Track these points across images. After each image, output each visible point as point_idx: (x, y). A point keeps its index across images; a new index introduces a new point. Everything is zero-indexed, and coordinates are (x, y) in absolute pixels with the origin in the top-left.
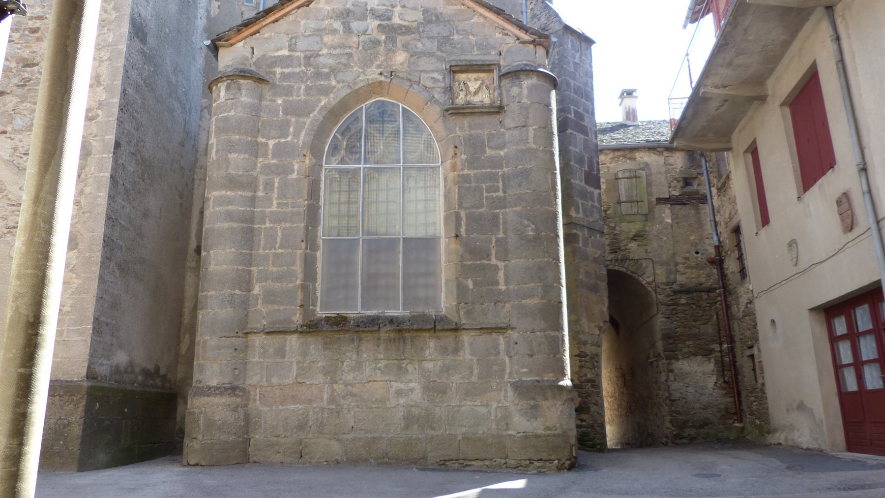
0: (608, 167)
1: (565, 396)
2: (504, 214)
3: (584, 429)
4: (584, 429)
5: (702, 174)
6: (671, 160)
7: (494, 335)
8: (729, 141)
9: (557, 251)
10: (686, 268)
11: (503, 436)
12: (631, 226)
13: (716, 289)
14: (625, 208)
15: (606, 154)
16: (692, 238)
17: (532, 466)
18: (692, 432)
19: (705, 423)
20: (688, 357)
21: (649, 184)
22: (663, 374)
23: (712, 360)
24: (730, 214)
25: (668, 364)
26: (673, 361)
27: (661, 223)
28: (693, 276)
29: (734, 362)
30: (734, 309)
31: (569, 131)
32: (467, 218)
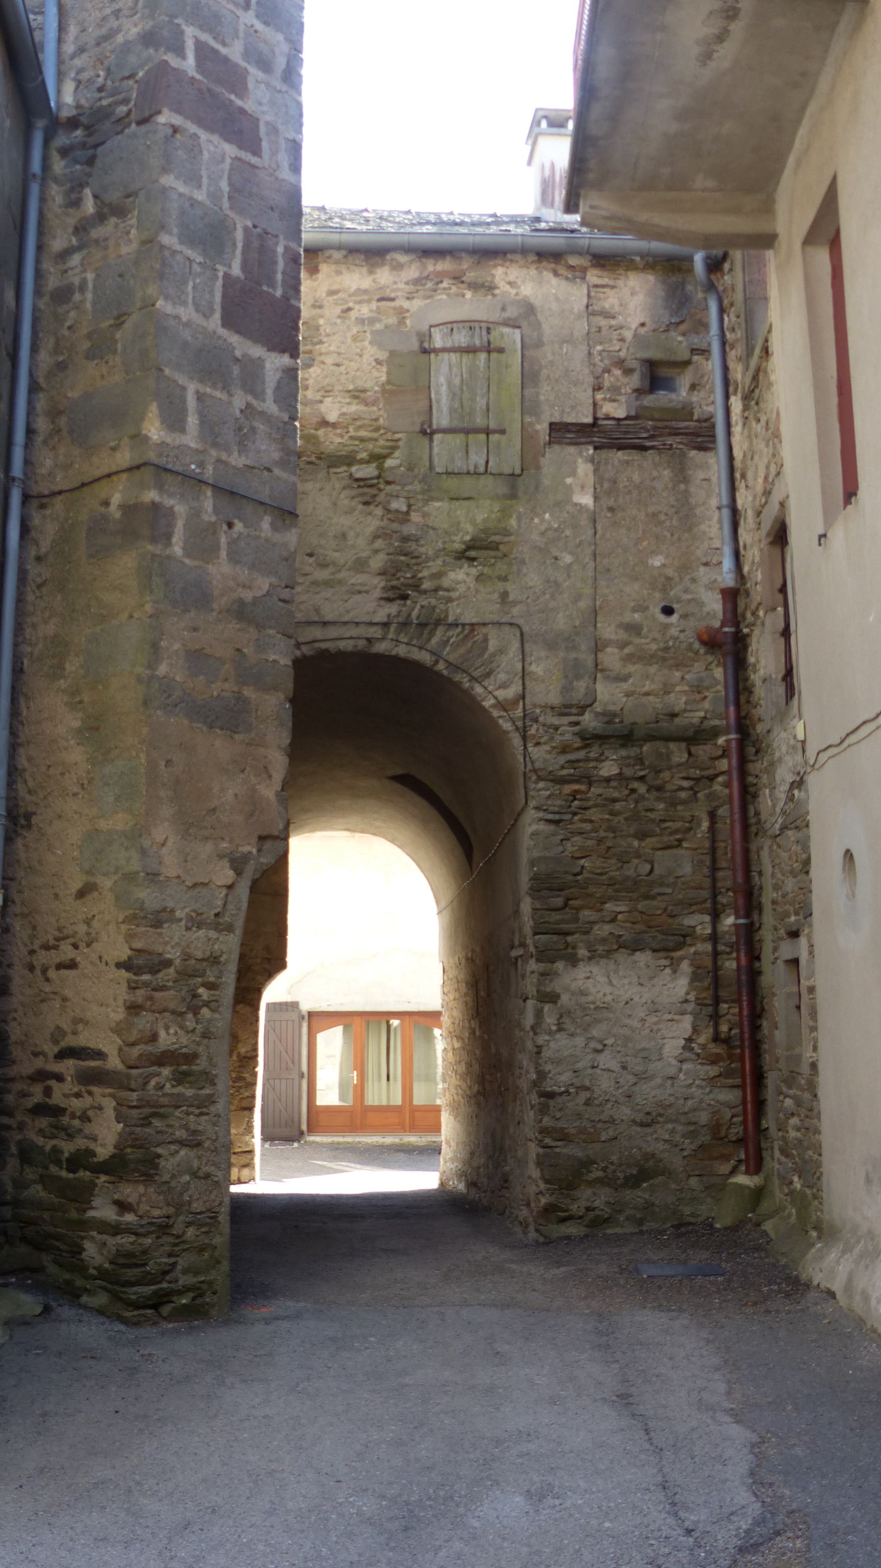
0: (401, 313)
3: (125, 1241)
4: (125, 1241)
5: (705, 352)
6: (610, 300)
8: (767, 208)
10: (629, 658)
12: (461, 510)
13: (715, 733)
14: (444, 451)
15: (398, 267)
16: (657, 561)
18: (599, 1199)
19: (644, 1172)
20: (608, 954)
21: (530, 376)
22: (530, 1003)
23: (685, 966)
24: (766, 478)
25: (542, 974)
26: (560, 965)
28: (648, 686)
29: (752, 973)
31: (165, 118)
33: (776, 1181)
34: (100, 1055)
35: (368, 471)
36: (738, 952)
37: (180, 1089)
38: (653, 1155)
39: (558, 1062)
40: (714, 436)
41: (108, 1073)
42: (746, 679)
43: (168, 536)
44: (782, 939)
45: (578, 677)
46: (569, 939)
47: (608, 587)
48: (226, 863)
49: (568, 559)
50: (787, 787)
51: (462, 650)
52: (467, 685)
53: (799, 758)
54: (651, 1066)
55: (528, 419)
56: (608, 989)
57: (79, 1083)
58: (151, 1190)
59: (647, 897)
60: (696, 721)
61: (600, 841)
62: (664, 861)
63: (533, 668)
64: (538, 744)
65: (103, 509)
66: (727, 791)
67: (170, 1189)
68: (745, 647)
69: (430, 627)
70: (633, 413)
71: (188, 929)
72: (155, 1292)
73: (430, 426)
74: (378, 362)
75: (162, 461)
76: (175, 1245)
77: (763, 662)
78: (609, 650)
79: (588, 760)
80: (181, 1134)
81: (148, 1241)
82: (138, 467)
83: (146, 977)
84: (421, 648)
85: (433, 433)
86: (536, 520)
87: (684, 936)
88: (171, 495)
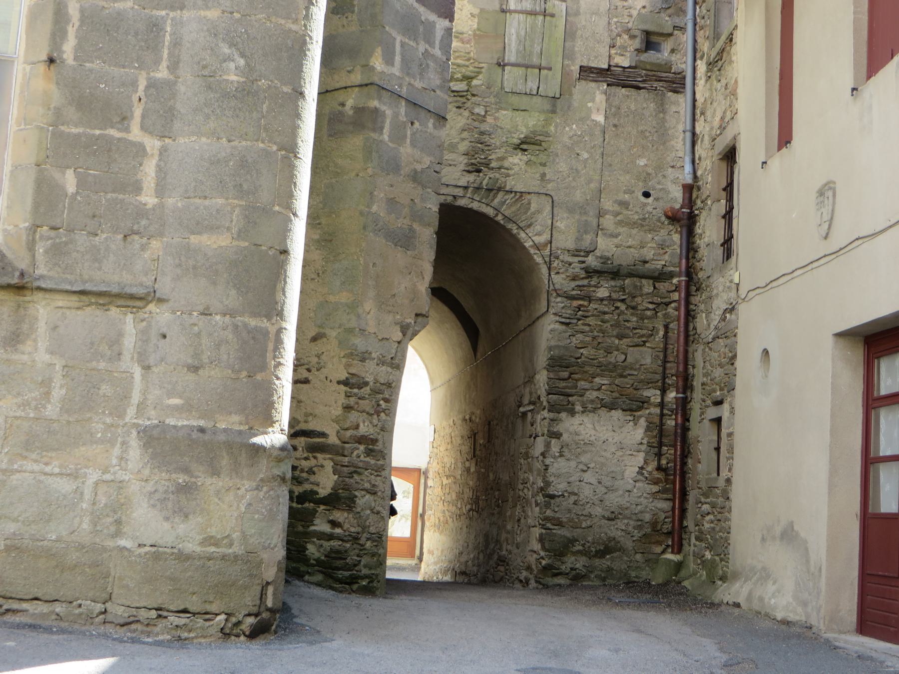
1: (264, 469)
2: (176, 23)
3: (335, 543)
4: (335, 543)
5: (682, 29)
7: (114, 312)
9: (294, 131)
10: (620, 223)
11: (105, 549)
12: (519, 117)
13: (671, 275)
14: (511, 78)
16: (642, 162)
17: (161, 624)
18: (580, 563)
19: (608, 549)
20: (594, 410)
21: (570, 34)
22: (540, 440)
24: (722, 119)
26: (563, 415)
27: (583, 120)
29: (684, 429)
30: (701, 321)
32: (82, 21)
33: (691, 558)
34: (323, 435)
35: (461, 86)
36: (676, 415)
37: (368, 459)
38: (614, 539)
39: (559, 476)
40: (684, 84)
41: (329, 445)
42: (694, 243)
43: (382, 128)
44: (707, 407)
45: (586, 232)
46: (570, 399)
47: (609, 176)
48: (398, 328)
49: (586, 155)
50: (721, 313)
51: (513, 209)
52: (515, 231)
53: (733, 294)
54: (617, 483)
55: (566, 62)
56: (593, 432)
57: (308, 451)
58: (351, 516)
59: (621, 376)
60: (659, 267)
61: (594, 338)
62: (634, 355)
63: (558, 224)
64: (558, 273)
65: (340, 108)
66: (676, 313)
67: (360, 516)
68: (694, 223)
69: (495, 192)
70: (634, 64)
71: (378, 365)
72: (351, 575)
73: (503, 61)
74: (472, 15)
75: (381, 83)
76: (361, 550)
77: (708, 233)
78: (607, 216)
79: (589, 286)
80: (367, 485)
81: (348, 545)
82: (366, 85)
83: (356, 390)
84: (487, 205)
85: (505, 65)
86: (567, 129)
87: (643, 403)
88: (385, 104)
